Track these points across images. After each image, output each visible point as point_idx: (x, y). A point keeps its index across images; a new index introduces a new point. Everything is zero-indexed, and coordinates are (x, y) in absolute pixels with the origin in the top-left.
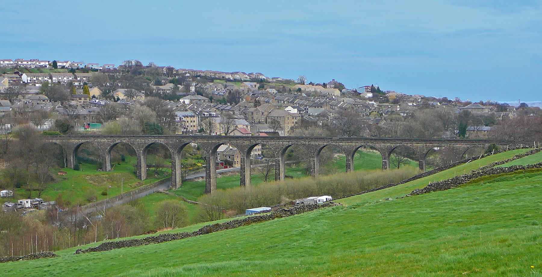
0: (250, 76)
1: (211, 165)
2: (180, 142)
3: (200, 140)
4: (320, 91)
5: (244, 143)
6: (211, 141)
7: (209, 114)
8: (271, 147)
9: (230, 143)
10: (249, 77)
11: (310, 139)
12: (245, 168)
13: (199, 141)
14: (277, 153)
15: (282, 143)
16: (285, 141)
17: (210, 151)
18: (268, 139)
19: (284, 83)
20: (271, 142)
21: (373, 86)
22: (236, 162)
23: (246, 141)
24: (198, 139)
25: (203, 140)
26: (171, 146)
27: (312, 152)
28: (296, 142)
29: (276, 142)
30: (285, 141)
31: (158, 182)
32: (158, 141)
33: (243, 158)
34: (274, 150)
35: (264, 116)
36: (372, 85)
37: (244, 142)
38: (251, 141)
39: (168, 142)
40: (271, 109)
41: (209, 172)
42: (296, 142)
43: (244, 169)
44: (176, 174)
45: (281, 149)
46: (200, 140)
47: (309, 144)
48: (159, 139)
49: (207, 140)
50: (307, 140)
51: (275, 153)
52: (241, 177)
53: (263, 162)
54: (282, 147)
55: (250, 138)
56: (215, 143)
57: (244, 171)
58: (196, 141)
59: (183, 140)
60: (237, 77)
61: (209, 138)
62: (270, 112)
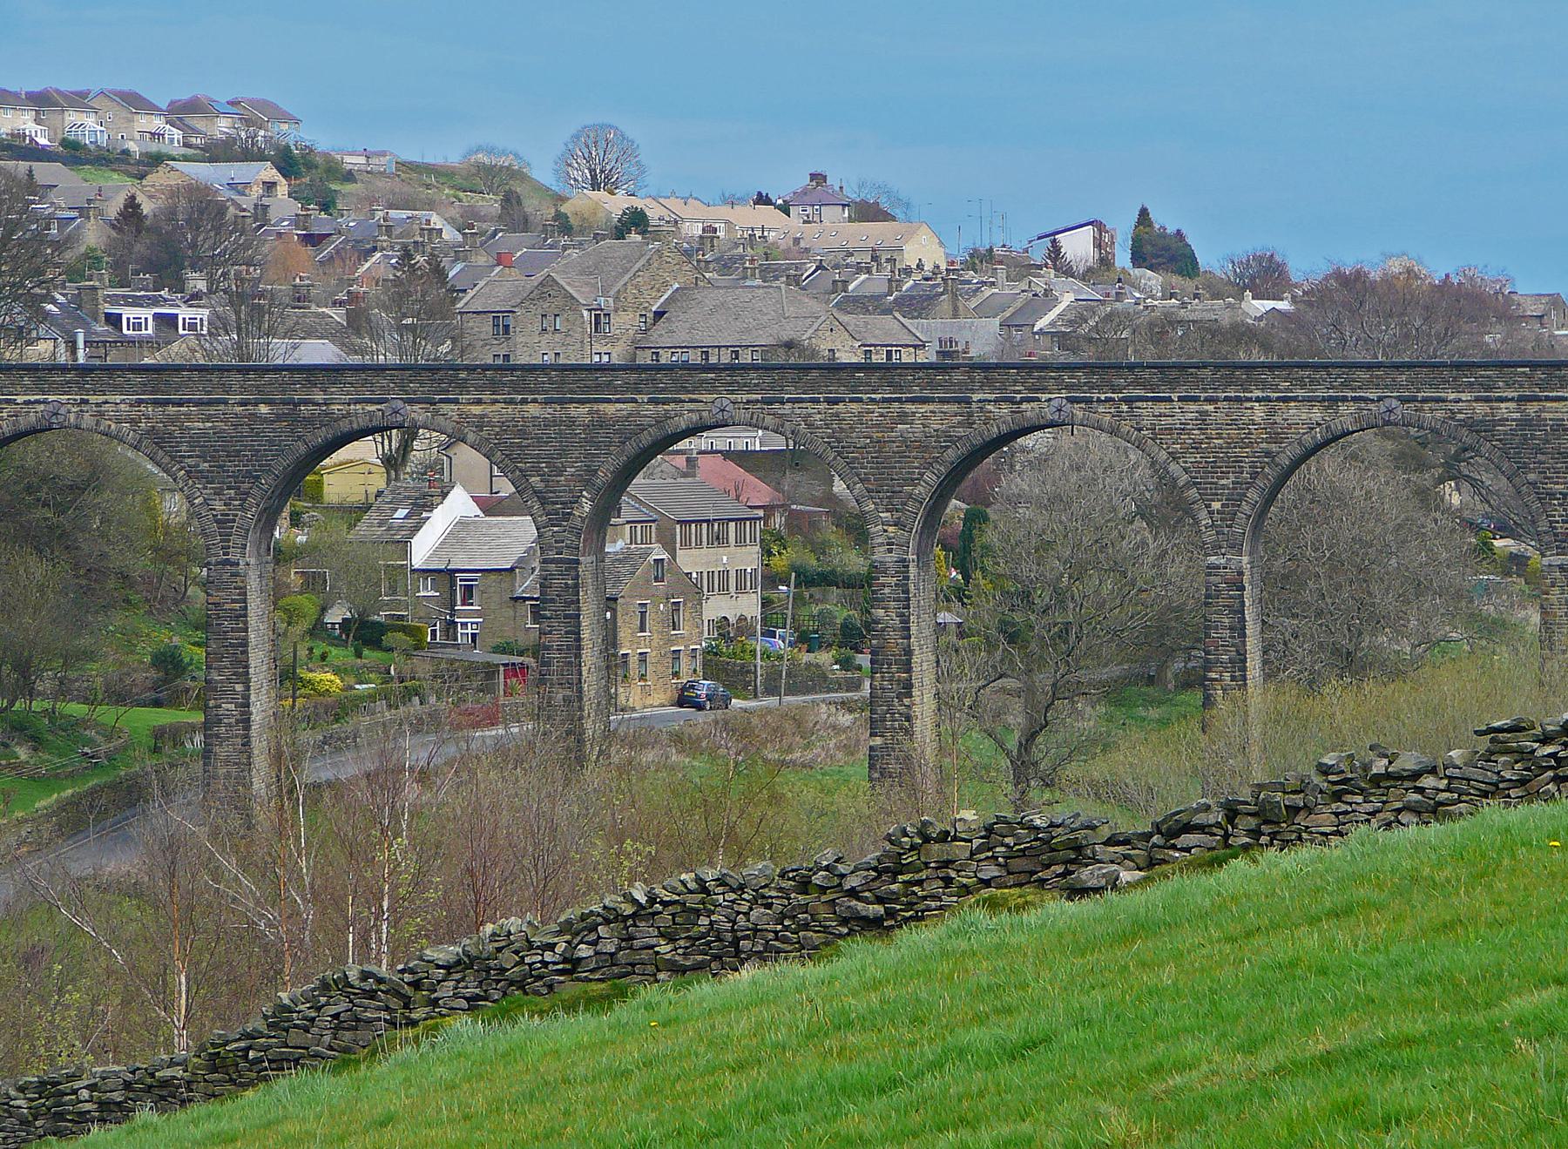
0: (188, 130)
1: (586, 634)
2: (290, 415)
3: (486, 397)
4: (797, 241)
5: (903, 417)
6: (584, 409)
7: (156, 316)
8: (1163, 455)
9: (769, 420)
10: (177, 134)
11: (1539, 374)
12: (909, 652)
13: (476, 410)
14: (1216, 505)
15: (1271, 412)
16: (1300, 393)
17: (576, 500)
18: (1137, 383)
19: (458, 180)
20: (1162, 408)
21: (1150, 225)
22: (633, 661)
23: (924, 401)
24: (463, 387)
25: (512, 402)
26: (203, 457)
27: (1552, 495)
28: (1403, 400)
29: (1210, 408)
30: (1300, 393)
31: (63, 806)
32: (80, 414)
33: (894, 556)
34: (1188, 485)
35: (614, 340)
36: (1144, 213)
37: (910, 407)
38: (968, 402)
39: (173, 420)
40: (666, 284)
41: (566, 700)
42: (1403, 400)
43: (909, 662)
44: (248, 728)
45: (1254, 475)
46: (479, 402)
47: (1525, 423)
48: (81, 390)
49: (547, 402)
50: (1508, 386)
51: (1203, 514)
52: (878, 741)
53: (825, 678)
54: (1268, 454)
55: (957, 376)
56: (624, 430)
57: (908, 686)
58: (445, 408)
59: (319, 397)
60: (87, 126)
61: (571, 376)
62: (659, 315)
